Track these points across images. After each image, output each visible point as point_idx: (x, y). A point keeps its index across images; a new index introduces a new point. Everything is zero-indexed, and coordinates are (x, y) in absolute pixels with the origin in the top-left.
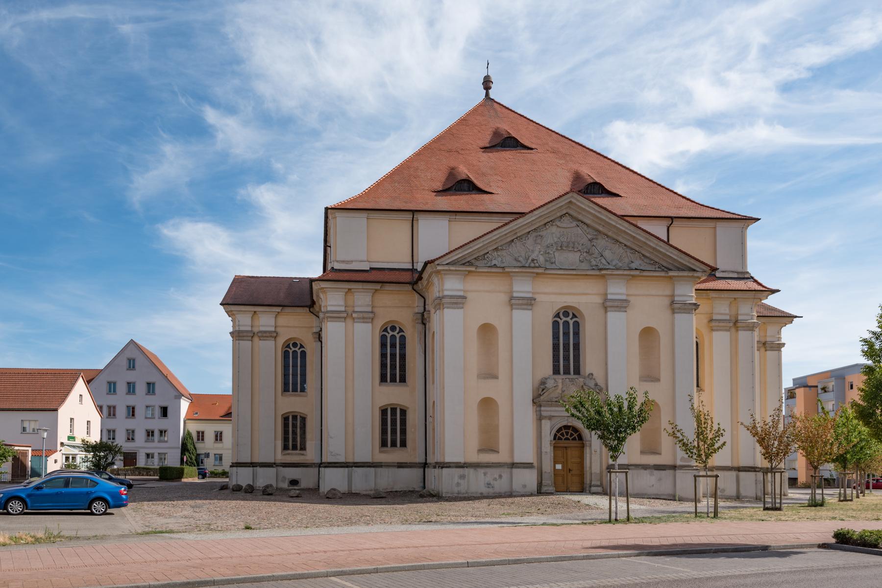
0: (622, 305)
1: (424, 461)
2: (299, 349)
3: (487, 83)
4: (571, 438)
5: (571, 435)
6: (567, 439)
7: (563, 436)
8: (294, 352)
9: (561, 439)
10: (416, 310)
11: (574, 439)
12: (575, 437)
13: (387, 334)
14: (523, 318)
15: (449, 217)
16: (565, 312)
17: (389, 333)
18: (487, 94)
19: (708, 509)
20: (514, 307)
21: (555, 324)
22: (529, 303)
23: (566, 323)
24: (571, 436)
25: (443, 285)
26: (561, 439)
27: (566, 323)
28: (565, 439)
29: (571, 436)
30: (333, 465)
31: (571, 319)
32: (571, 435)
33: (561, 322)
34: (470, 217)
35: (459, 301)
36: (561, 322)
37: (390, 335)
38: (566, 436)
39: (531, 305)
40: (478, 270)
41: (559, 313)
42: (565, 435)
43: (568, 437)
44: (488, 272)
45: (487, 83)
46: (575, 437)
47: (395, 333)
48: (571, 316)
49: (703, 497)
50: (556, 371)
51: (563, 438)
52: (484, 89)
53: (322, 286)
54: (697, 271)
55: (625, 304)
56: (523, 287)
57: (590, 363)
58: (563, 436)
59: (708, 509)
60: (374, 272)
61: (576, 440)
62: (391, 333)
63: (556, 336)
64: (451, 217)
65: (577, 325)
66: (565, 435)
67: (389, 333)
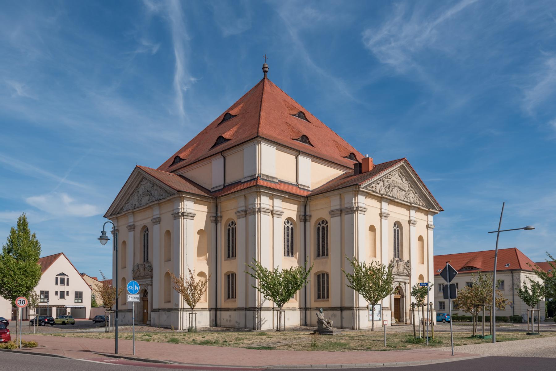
40: (160, 202)
48: (319, 226)
60: (282, 184)
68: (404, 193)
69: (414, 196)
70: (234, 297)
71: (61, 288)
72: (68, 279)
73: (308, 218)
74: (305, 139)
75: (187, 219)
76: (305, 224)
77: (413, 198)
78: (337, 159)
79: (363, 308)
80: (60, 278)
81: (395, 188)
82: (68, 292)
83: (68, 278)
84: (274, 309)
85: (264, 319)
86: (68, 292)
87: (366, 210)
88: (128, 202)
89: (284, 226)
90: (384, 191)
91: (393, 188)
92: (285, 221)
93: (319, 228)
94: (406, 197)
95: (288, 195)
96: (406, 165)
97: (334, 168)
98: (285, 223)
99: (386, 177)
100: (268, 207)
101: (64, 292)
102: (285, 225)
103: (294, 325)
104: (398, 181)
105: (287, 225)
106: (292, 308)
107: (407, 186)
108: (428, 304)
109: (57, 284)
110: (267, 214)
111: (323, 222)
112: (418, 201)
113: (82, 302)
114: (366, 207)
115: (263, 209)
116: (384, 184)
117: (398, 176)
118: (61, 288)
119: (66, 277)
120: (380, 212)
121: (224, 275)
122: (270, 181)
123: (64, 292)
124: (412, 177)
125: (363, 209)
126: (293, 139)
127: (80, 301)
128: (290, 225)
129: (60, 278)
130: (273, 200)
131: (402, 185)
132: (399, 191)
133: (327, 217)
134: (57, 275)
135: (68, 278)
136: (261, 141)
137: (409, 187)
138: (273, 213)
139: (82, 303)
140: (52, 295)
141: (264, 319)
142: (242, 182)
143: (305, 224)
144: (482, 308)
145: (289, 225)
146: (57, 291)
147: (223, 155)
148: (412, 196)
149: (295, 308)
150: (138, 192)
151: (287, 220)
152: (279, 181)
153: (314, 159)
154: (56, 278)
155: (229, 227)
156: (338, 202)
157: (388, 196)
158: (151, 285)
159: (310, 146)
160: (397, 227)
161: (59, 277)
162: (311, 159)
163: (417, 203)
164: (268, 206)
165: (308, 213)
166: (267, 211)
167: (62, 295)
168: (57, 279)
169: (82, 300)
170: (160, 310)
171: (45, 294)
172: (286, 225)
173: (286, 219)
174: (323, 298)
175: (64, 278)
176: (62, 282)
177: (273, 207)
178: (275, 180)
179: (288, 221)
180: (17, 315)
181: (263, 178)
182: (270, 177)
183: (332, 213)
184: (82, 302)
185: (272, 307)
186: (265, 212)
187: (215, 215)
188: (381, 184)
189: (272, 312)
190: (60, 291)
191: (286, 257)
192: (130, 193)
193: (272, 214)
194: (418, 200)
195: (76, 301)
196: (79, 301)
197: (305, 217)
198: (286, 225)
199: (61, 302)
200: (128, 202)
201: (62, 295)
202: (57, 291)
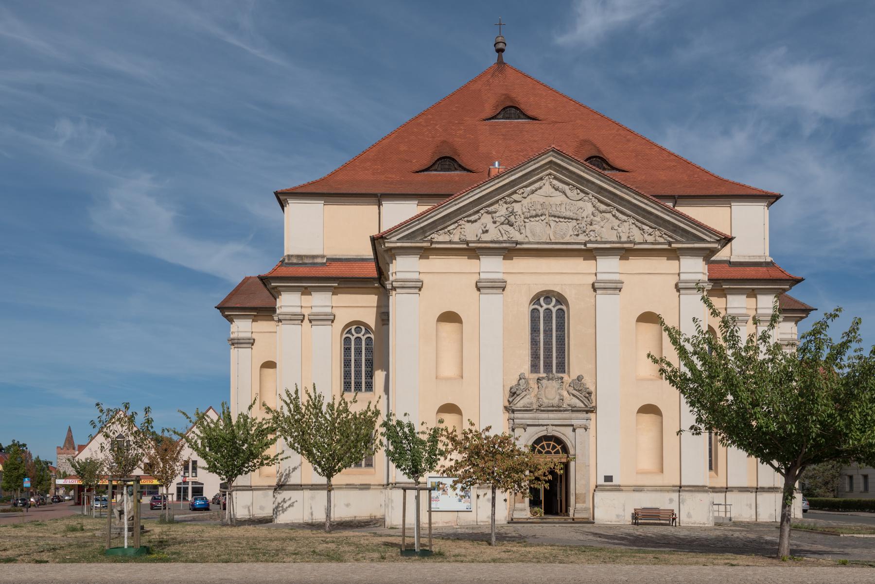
0: (616, 288)
2: (542, 307)
4: (553, 452)
5: (554, 447)
6: (548, 452)
7: (544, 449)
9: (542, 453)
11: (557, 452)
12: (553, 445)
13: (539, 307)
14: (492, 301)
16: (548, 295)
17: (353, 335)
19: (404, 540)
21: (534, 314)
22: (500, 286)
23: (358, 339)
24: (553, 449)
26: (542, 453)
27: (358, 339)
28: (546, 453)
29: (553, 449)
30: (318, 487)
32: (554, 447)
37: (354, 337)
38: (547, 449)
42: (551, 448)
43: (550, 450)
46: (553, 445)
47: (550, 307)
50: (535, 368)
51: (544, 451)
55: (619, 285)
57: (577, 364)
58: (544, 449)
59: (404, 540)
60: (334, 264)
61: (559, 453)
62: (545, 306)
63: (534, 330)
65: (561, 314)
66: (551, 448)
68: (574, 223)
75: (239, 349)
79: (246, 488)
84: (683, 488)
85: (290, 499)
87: (621, 285)
90: (497, 231)
96: (562, 161)
97: (714, 205)
103: (362, 515)
104: (553, 200)
106: (361, 485)
115: (284, 316)
117: (553, 190)
122: (306, 264)
124: (593, 183)
126: (417, 172)
130: (756, 298)
133: (722, 315)
141: (290, 499)
144: (57, 493)
149: (619, 486)
152: (328, 259)
157: (646, 243)
159: (465, 173)
162: (323, 202)
178: (319, 260)
181: (290, 262)
182: (307, 257)
185: (725, 486)
186: (291, 320)
189: (754, 494)
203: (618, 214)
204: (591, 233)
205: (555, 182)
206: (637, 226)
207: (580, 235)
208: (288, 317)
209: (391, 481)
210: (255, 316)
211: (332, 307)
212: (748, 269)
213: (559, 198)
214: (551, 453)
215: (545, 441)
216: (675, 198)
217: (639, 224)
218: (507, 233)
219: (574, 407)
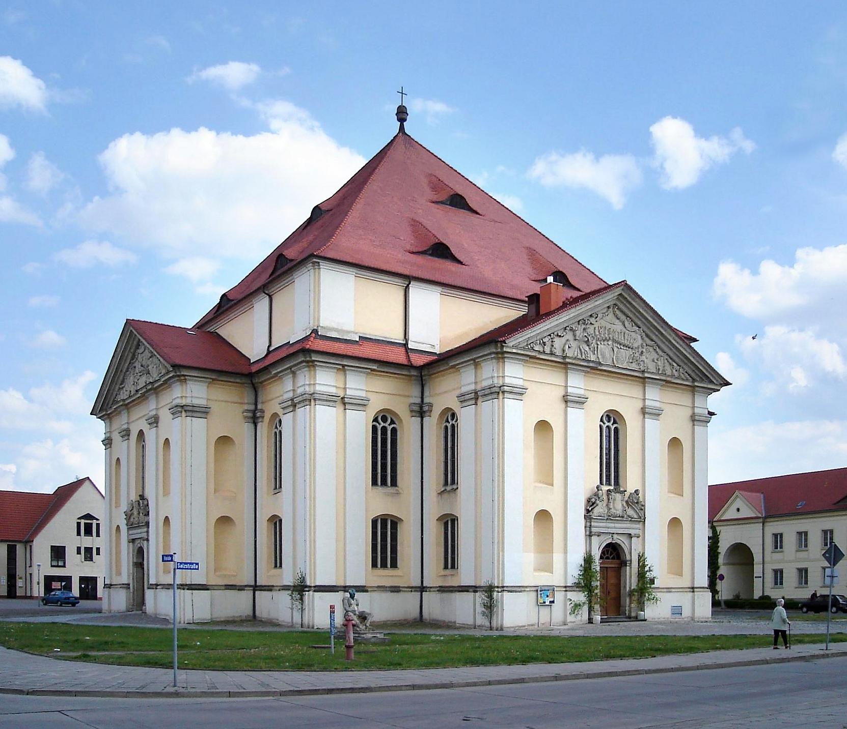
1: (766, 524)
3: (402, 114)
8: (608, 427)
10: (246, 407)
15: (441, 289)
17: (379, 424)
18: (402, 128)
20: (347, 407)
21: (374, 429)
23: (384, 429)
25: (315, 378)
27: (384, 429)
31: (389, 425)
33: (379, 428)
34: (485, 299)
35: (519, 393)
36: (379, 428)
37: (381, 426)
39: (207, 413)
41: (377, 417)
44: (555, 366)
45: (402, 114)
47: (386, 425)
49: (148, 588)
52: (399, 120)
53: (313, 359)
54: (715, 384)
56: (577, 383)
60: (366, 343)
62: (383, 424)
64: (443, 290)
65: (394, 431)
67: (379, 424)
68: (631, 352)
69: (656, 356)
70: (456, 567)
71: (87, 542)
72: (98, 525)
73: (426, 408)
74: (441, 251)
76: (422, 420)
77: (651, 361)
78: (513, 287)
80: (85, 523)
81: (606, 343)
82: (78, 554)
83: (99, 524)
86: (98, 549)
87: (661, 412)
88: (123, 386)
89: (601, 427)
91: (599, 343)
92: (602, 416)
93: (446, 427)
94: (633, 360)
95: (376, 365)
98: (602, 420)
99: (581, 322)
100: (333, 391)
101: (92, 548)
102: (601, 423)
105: (607, 424)
107: (639, 337)
108: (831, 585)
109: (79, 534)
110: (331, 404)
111: (384, 419)
112: (668, 368)
113: (64, 566)
114: (526, 384)
116: (575, 336)
118: (87, 542)
119: (95, 522)
120: (563, 393)
121: (265, 523)
123: (92, 548)
125: (515, 389)
127: (61, 563)
128: (612, 425)
129: (85, 523)
131: (624, 336)
132: (615, 349)
133: (454, 405)
134: (79, 519)
135: (99, 524)
136: (319, 263)
137: (643, 339)
138: (344, 402)
139: (65, 567)
140: (70, 553)
142: (291, 343)
143: (422, 420)
145: (610, 424)
146: (80, 547)
147: (267, 292)
148: (652, 358)
149: (399, 587)
150: (135, 367)
151: (606, 414)
153: (447, 290)
154: (77, 522)
155: (276, 430)
156: (472, 379)
158: (148, 540)
160: (615, 422)
161: (83, 522)
163: (664, 370)
164: (335, 388)
165: (426, 400)
166: (330, 400)
167: (88, 554)
168: (79, 524)
169: (65, 563)
170: (158, 587)
171: (58, 553)
172: (604, 423)
173: (605, 412)
174: (452, 568)
175: (92, 523)
176: (88, 531)
177: (345, 389)
179: (607, 415)
180: (792, 602)
183: (463, 399)
184: (64, 566)
187: (252, 407)
188: (569, 336)
190: (85, 548)
191: (380, 490)
192: (124, 371)
193: (344, 404)
194: (667, 364)
195: (55, 563)
196: (59, 564)
197: (421, 407)
198: (604, 423)
199: (88, 570)
200: (123, 386)
201: (88, 554)
202: (80, 547)
203: (658, 350)
204: (642, 363)
205: (618, 312)
206: (668, 361)
207: (634, 363)
208: (325, 397)
209: (258, 584)
210: (213, 380)
211: (208, 399)
212: (327, 343)
213: (618, 327)
214: (609, 559)
215: (612, 549)
216: (409, 279)
217: (670, 361)
218: (585, 352)
219: (632, 518)
